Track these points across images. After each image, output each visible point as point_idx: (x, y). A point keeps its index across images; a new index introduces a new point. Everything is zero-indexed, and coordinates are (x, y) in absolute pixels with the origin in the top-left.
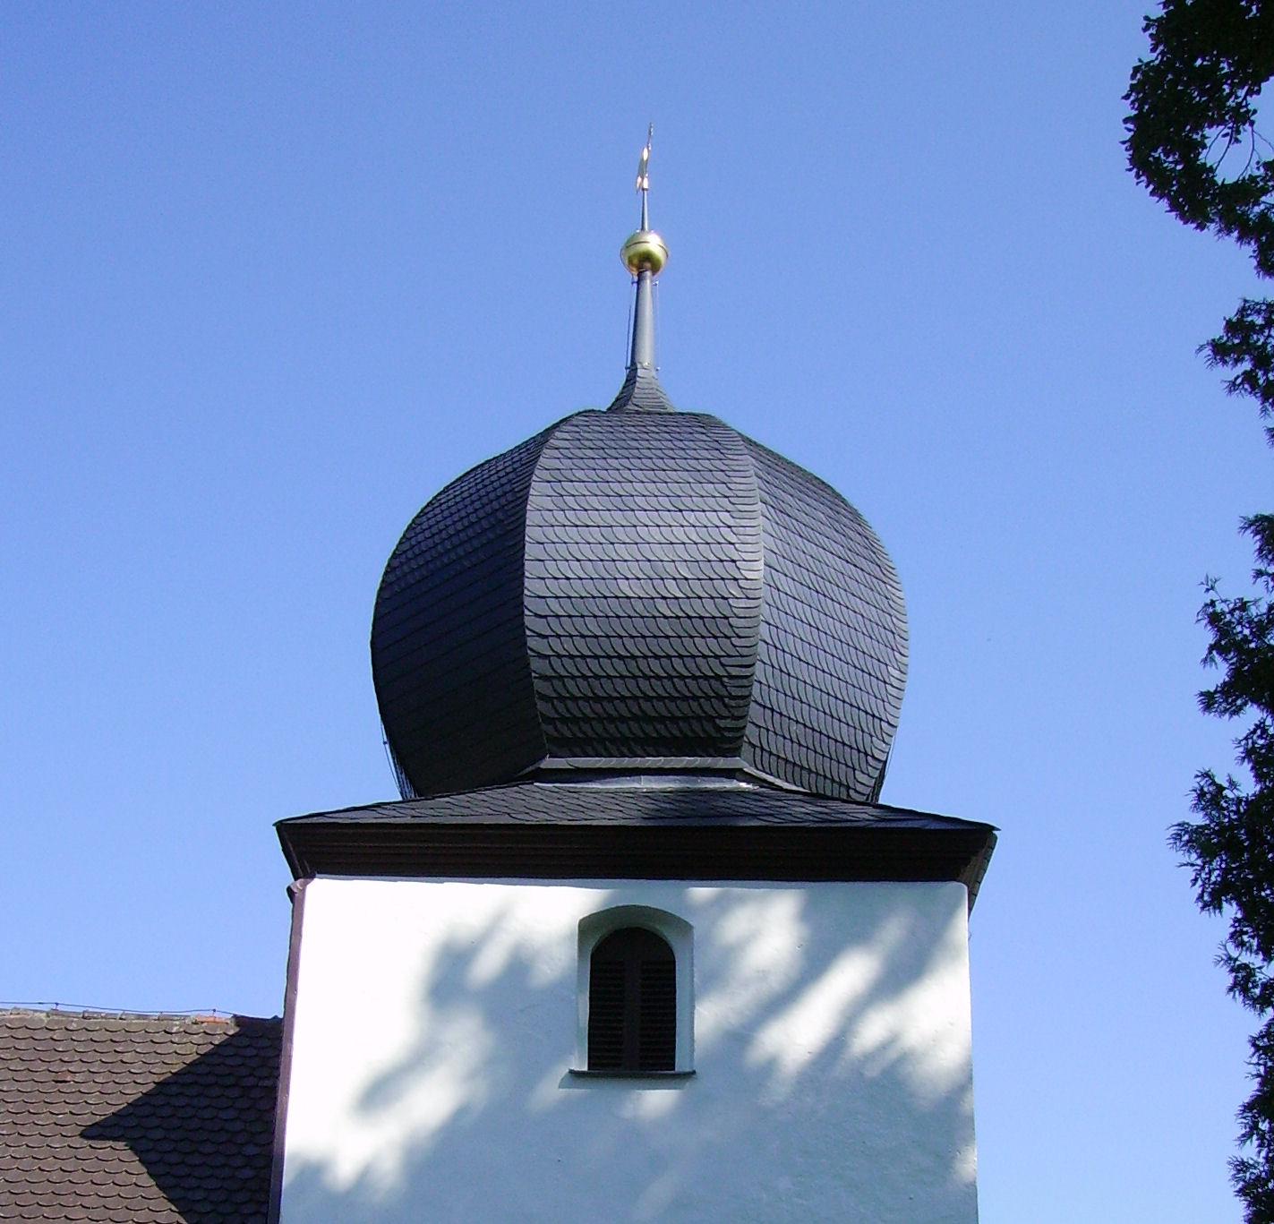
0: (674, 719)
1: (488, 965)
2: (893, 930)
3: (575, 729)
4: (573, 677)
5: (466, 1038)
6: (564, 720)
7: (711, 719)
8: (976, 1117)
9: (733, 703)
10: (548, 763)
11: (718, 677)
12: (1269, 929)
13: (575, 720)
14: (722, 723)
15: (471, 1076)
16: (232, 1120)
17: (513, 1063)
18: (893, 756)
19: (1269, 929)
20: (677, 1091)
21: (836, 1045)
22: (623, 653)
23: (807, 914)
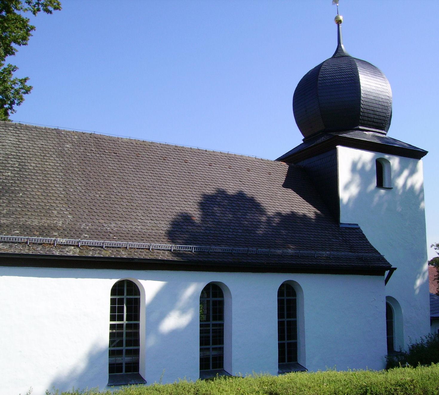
0: (378, 123)
1: (359, 166)
2: (410, 166)
3: (374, 123)
4: (366, 113)
5: (357, 179)
6: (363, 120)
7: (382, 124)
8: (424, 190)
9: (386, 122)
10: (360, 127)
11: (385, 117)
12: (363, 394)
13: (364, 120)
14: (383, 124)
15: (358, 186)
16: (200, 241)
17: (364, 184)
18: (149, 140)
19: (363, 394)
20: (385, 191)
21: (405, 185)
22: (373, 110)
23: (400, 163)
